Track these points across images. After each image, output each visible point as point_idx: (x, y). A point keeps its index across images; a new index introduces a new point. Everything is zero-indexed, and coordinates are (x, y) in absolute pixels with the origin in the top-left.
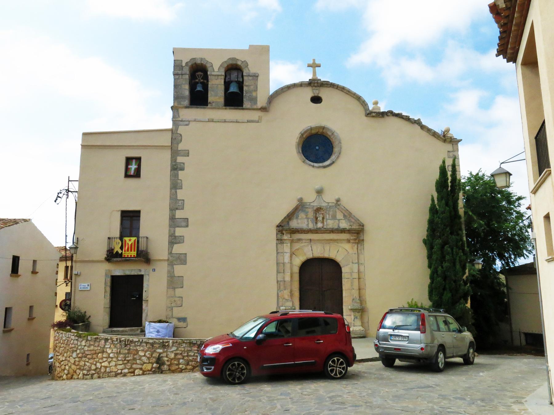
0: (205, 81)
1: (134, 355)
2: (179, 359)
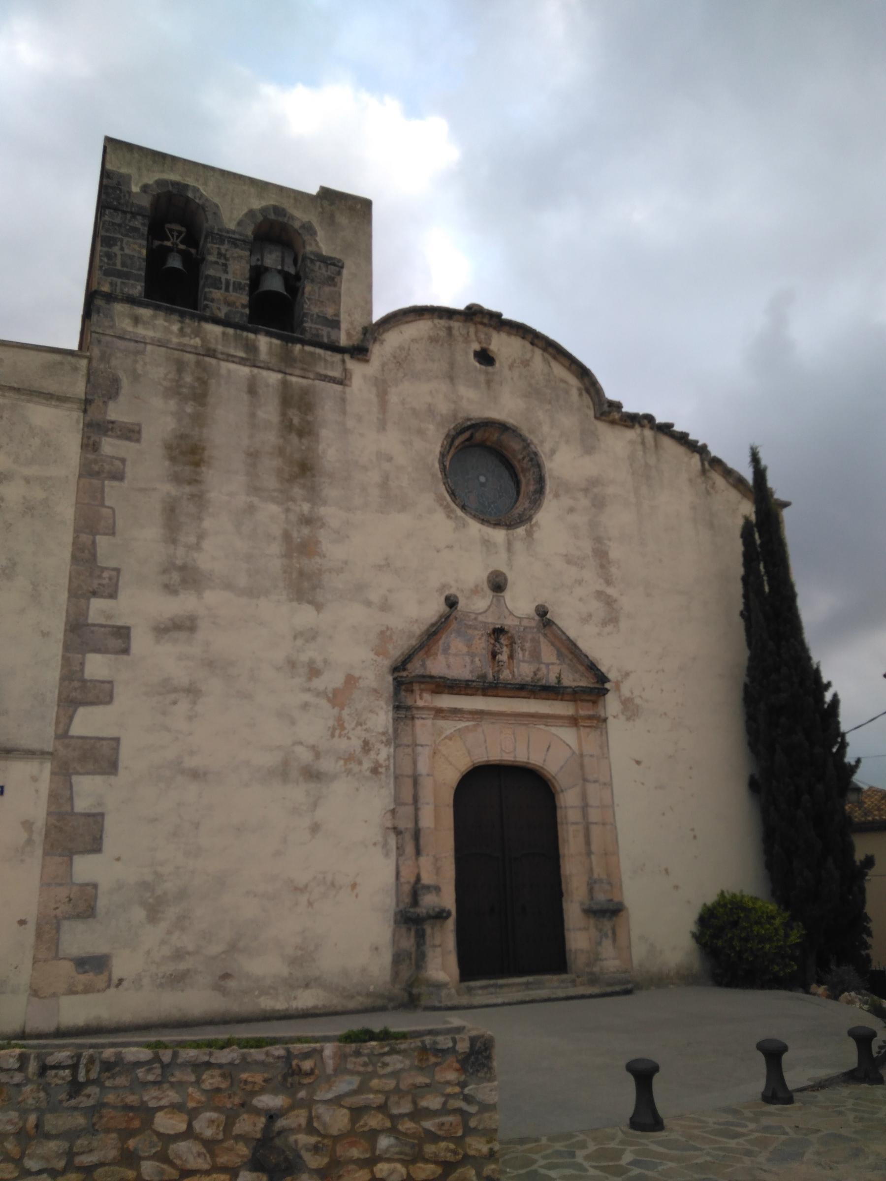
0: (193, 251)
1: (127, 1134)
2: (373, 1135)
